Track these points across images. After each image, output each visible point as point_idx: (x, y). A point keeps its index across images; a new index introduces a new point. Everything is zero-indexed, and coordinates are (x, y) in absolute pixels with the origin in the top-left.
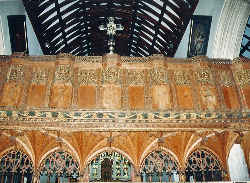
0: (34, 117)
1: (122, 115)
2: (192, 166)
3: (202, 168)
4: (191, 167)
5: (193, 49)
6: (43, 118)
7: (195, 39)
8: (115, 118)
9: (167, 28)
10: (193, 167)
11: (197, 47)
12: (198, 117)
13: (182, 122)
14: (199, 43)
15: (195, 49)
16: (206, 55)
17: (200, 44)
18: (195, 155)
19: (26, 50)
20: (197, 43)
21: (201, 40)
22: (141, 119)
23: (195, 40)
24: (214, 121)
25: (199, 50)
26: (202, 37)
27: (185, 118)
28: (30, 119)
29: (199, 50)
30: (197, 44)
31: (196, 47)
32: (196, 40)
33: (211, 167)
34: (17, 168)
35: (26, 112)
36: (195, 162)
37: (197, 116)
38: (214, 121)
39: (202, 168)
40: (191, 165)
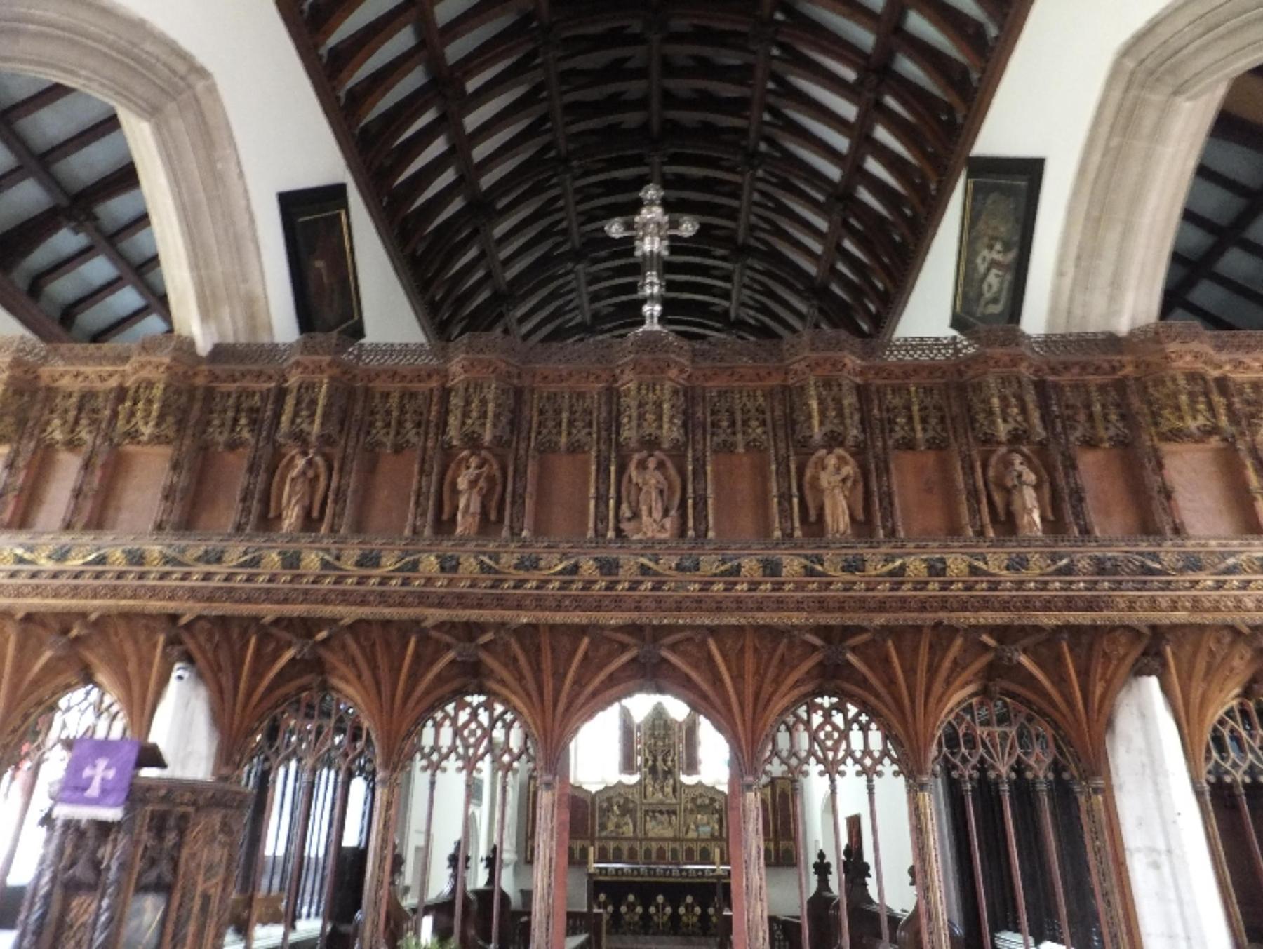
2: (1230, 762)
3: (1003, 768)
4: (1227, 765)
5: (972, 294)
8: (661, 575)
11: (985, 287)
12: (974, 571)
14: (994, 271)
15: (981, 294)
17: (997, 276)
18: (1233, 718)
19: (352, 317)
20: (988, 270)
21: (999, 257)
22: (758, 576)
23: (979, 260)
25: (995, 300)
26: (1007, 248)
27: (923, 574)
29: (995, 300)
31: (980, 287)
32: (984, 259)
33: (1235, 765)
36: (971, 742)
37: (805, 567)
38: (706, 586)
39: (1003, 768)
40: (953, 754)
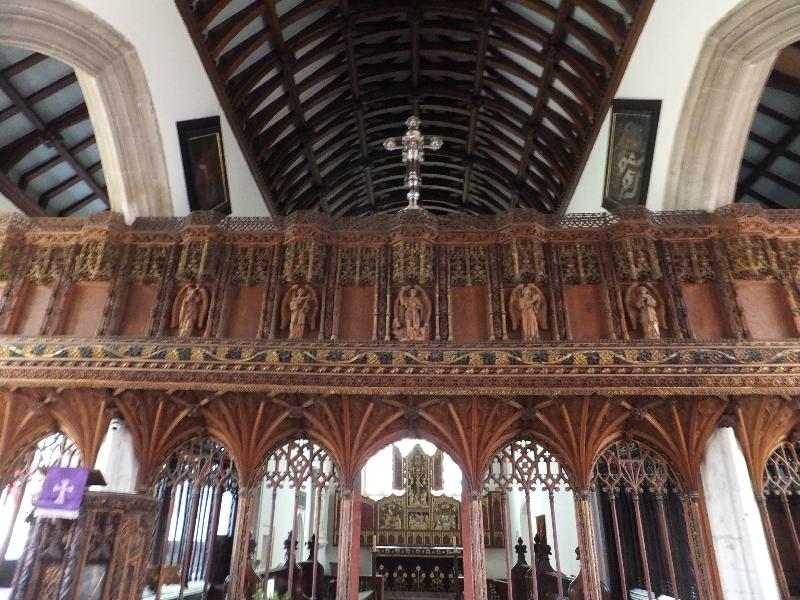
0: (239, 361)
1: (435, 356)
4: (777, 484)
6: (258, 363)
7: (619, 161)
9: (233, 129)
10: (611, 481)
11: (624, 181)
12: (617, 361)
13: (444, 373)
14: (630, 171)
15: (621, 186)
16: (645, 204)
17: (631, 174)
20: (626, 170)
21: (633, 163)
24: (447, 370)
25: (630, 190)
26: (637, 157)
28: (230, 367)
29: (630, 190)
30: (624, 174)
31: (621, 182)
33: (782, 484)
34: (641, 481)
35: (223, 351)
36: (615, 469)
40: (603, 476)
